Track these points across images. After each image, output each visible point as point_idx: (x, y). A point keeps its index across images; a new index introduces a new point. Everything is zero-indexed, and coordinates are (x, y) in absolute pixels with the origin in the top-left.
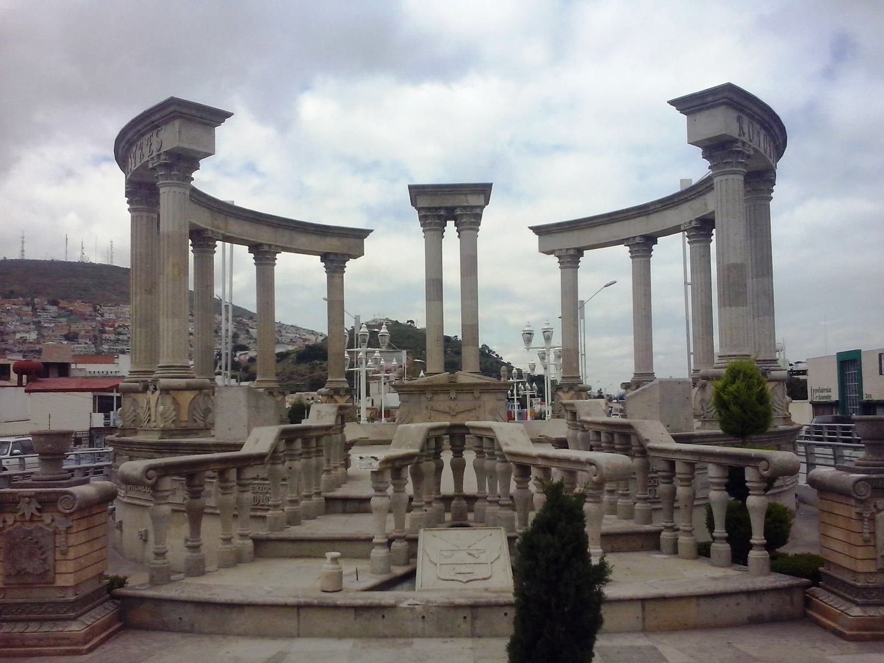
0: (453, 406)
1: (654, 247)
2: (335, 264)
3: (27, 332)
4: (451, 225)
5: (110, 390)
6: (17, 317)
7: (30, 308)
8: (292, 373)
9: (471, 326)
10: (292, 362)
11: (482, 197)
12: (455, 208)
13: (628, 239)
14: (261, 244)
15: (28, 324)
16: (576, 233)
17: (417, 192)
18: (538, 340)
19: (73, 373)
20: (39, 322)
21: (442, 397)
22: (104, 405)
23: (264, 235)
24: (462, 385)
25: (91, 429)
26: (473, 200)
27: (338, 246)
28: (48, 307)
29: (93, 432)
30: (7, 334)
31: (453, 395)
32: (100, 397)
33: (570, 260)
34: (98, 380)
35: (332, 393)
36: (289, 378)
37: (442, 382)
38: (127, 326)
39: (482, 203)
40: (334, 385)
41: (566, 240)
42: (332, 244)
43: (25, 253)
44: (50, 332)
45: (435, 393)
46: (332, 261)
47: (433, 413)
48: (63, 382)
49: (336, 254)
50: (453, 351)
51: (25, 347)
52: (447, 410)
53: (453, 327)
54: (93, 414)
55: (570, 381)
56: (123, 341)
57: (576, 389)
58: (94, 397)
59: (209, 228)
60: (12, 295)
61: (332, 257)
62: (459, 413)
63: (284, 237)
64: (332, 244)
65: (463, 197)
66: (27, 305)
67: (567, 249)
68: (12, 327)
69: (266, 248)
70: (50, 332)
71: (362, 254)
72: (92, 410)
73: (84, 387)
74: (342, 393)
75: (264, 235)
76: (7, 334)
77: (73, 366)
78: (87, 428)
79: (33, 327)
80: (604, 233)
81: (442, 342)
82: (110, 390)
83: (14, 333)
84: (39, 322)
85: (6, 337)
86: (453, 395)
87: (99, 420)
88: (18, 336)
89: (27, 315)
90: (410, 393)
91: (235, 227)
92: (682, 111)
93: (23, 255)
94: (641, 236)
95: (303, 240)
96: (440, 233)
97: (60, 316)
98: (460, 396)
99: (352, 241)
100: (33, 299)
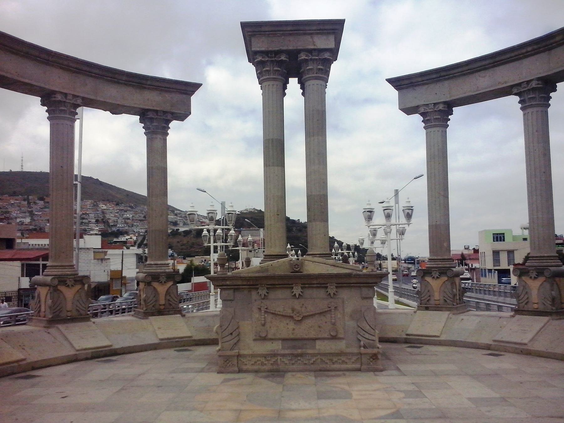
0: (297, 307)
1: (552, 94)
2: (156, 123)
3: (24, 218)
5: (37, 259)
6: (18, 208)
7: (26, 203)
8: (193, 244)
9: (318, 201)
10: (194, 237)
11: (332, 38)
12: (299, 51)
13: (519, 85)
14: (54, 92)
15: (25, 213)
16: (446, 83)
17: (253, 31)
18: (379, 219)
20: (32, 211)
21: (280, 294)
22: (30, 270)
23: (58, 81)
24: (310, 277)
25: (20, 289)
26: (322, 42)
27: (161, 103)
28: (38, 202)
29: (21, 292)
30: (12, 219)
31: (297, 290)
32: (27, 264)
33: (436, 117)
34: (28, 252)
35: (149, 279)
36: (191, 247)
37: (279, 273)
38: (88, 214)
39: (332, 45)
40: (153, 270)
41: (434, 95)
42: (152, 99)
43: (23, 167)
44: (39, 218)
45: (272, 287)
46: (151, 120)
47: (269, 318)
49: (156, 111)
50: (296, 234)
51: (23, 227)
52: (289, 312)
53: (297, 209)
54: (21, 278)
55: (441, 264)
56: (85, 223)
57: (449, 273)
58: (23, 265)
60: (14, 194)
61: (151, 115)
62: (305, 317)
63: (85, 86)
64: (152, 99)
65: (308, 38)
66: (24, 200)
67: (435, 104)
68: (15, 215)
69: (59, 97)
70: (39, 218)
72: (20, 275)
73: (16, 257)
74: (163, 279)
76: (12, 219)
77: (18, 241)
78: (16, 288)
79: (27, 214)
80: (484, 81)
81: (284, 221)
82: (37, 259)
83: (16, 218)
84: (32, 211)
85: (10, 221)
86: (297, 290)
87: (25, 283)
88: (18, 220)
89: (24, 207)
90: (236, 289)
93: (22, 168)
94: (539, 79)
95: (112, 92)
96: (280, 84)
97: (45, 207)
98: (308, 292)
99: (176, 97)
100: (28, 196)
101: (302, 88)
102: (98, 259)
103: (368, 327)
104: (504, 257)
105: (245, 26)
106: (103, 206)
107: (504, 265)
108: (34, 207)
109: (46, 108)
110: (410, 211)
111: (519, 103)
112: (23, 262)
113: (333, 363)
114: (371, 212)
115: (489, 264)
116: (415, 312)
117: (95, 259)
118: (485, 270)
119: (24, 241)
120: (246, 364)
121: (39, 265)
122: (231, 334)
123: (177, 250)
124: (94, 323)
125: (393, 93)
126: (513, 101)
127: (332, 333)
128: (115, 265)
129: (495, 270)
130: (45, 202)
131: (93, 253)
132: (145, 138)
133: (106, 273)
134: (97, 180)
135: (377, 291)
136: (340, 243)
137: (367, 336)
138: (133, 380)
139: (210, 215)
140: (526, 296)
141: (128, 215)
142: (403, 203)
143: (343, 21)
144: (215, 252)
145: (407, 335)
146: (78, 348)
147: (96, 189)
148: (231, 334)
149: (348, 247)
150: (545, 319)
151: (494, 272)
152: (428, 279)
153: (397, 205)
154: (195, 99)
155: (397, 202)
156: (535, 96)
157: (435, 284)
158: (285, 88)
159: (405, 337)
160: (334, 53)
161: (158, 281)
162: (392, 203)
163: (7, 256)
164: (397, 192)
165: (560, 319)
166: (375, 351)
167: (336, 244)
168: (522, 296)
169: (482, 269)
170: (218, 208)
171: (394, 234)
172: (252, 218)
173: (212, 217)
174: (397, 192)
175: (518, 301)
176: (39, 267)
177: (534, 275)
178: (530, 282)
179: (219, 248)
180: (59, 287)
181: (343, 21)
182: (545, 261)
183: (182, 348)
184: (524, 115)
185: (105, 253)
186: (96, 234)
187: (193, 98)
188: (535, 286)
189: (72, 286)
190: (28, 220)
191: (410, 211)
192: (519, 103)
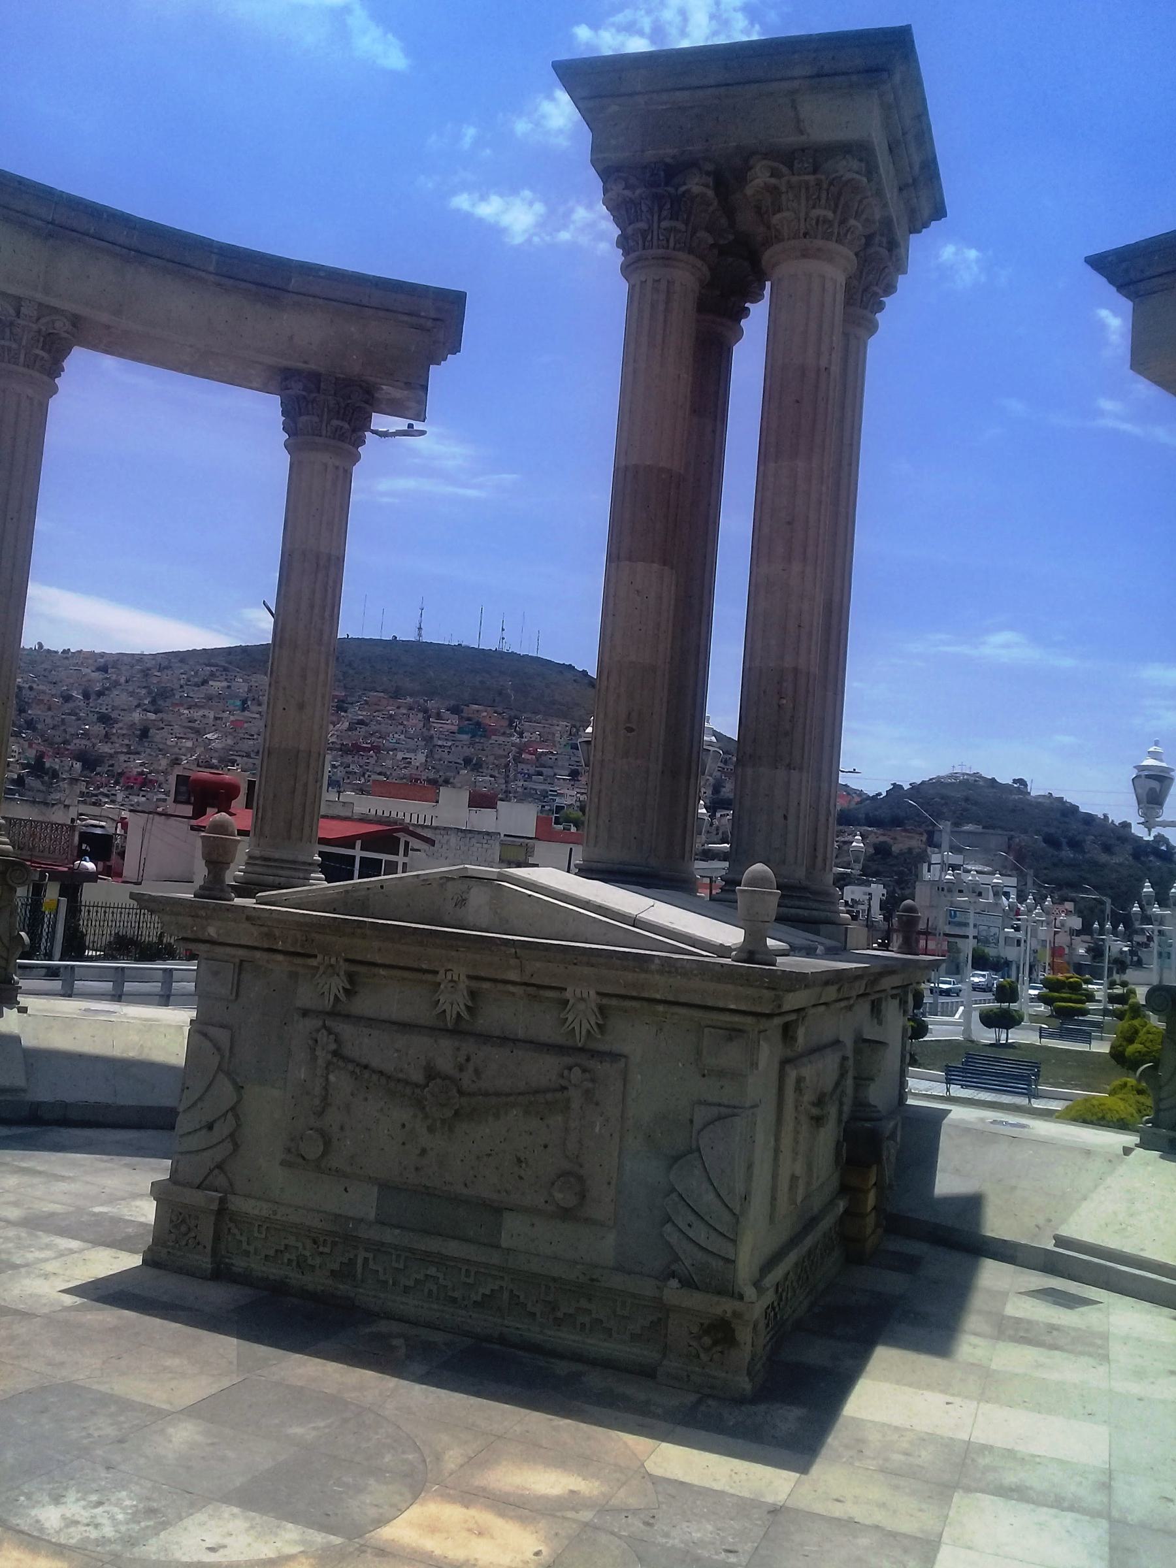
3: (414, 751)
5: (348, 842)
20: (432, 737)
63: (80, 280)
93: (420, 635)
97: (461, 731)
103: (711, 1196)
113: (558, 1322)
116: (1127, 1151)
120: (247, 1254)
121: (354, 857)
122: (210, 1127)
124: (23, 1010)
125: (1114, 319)
130: (461, 718)
132: (286, 458)
137: (701, 1234)
145: (1060, 1241)
148: (210, 1127)
159: (1050, 1245)
166: (724, 1307)
176: (353, 865)
190: (420, 758)
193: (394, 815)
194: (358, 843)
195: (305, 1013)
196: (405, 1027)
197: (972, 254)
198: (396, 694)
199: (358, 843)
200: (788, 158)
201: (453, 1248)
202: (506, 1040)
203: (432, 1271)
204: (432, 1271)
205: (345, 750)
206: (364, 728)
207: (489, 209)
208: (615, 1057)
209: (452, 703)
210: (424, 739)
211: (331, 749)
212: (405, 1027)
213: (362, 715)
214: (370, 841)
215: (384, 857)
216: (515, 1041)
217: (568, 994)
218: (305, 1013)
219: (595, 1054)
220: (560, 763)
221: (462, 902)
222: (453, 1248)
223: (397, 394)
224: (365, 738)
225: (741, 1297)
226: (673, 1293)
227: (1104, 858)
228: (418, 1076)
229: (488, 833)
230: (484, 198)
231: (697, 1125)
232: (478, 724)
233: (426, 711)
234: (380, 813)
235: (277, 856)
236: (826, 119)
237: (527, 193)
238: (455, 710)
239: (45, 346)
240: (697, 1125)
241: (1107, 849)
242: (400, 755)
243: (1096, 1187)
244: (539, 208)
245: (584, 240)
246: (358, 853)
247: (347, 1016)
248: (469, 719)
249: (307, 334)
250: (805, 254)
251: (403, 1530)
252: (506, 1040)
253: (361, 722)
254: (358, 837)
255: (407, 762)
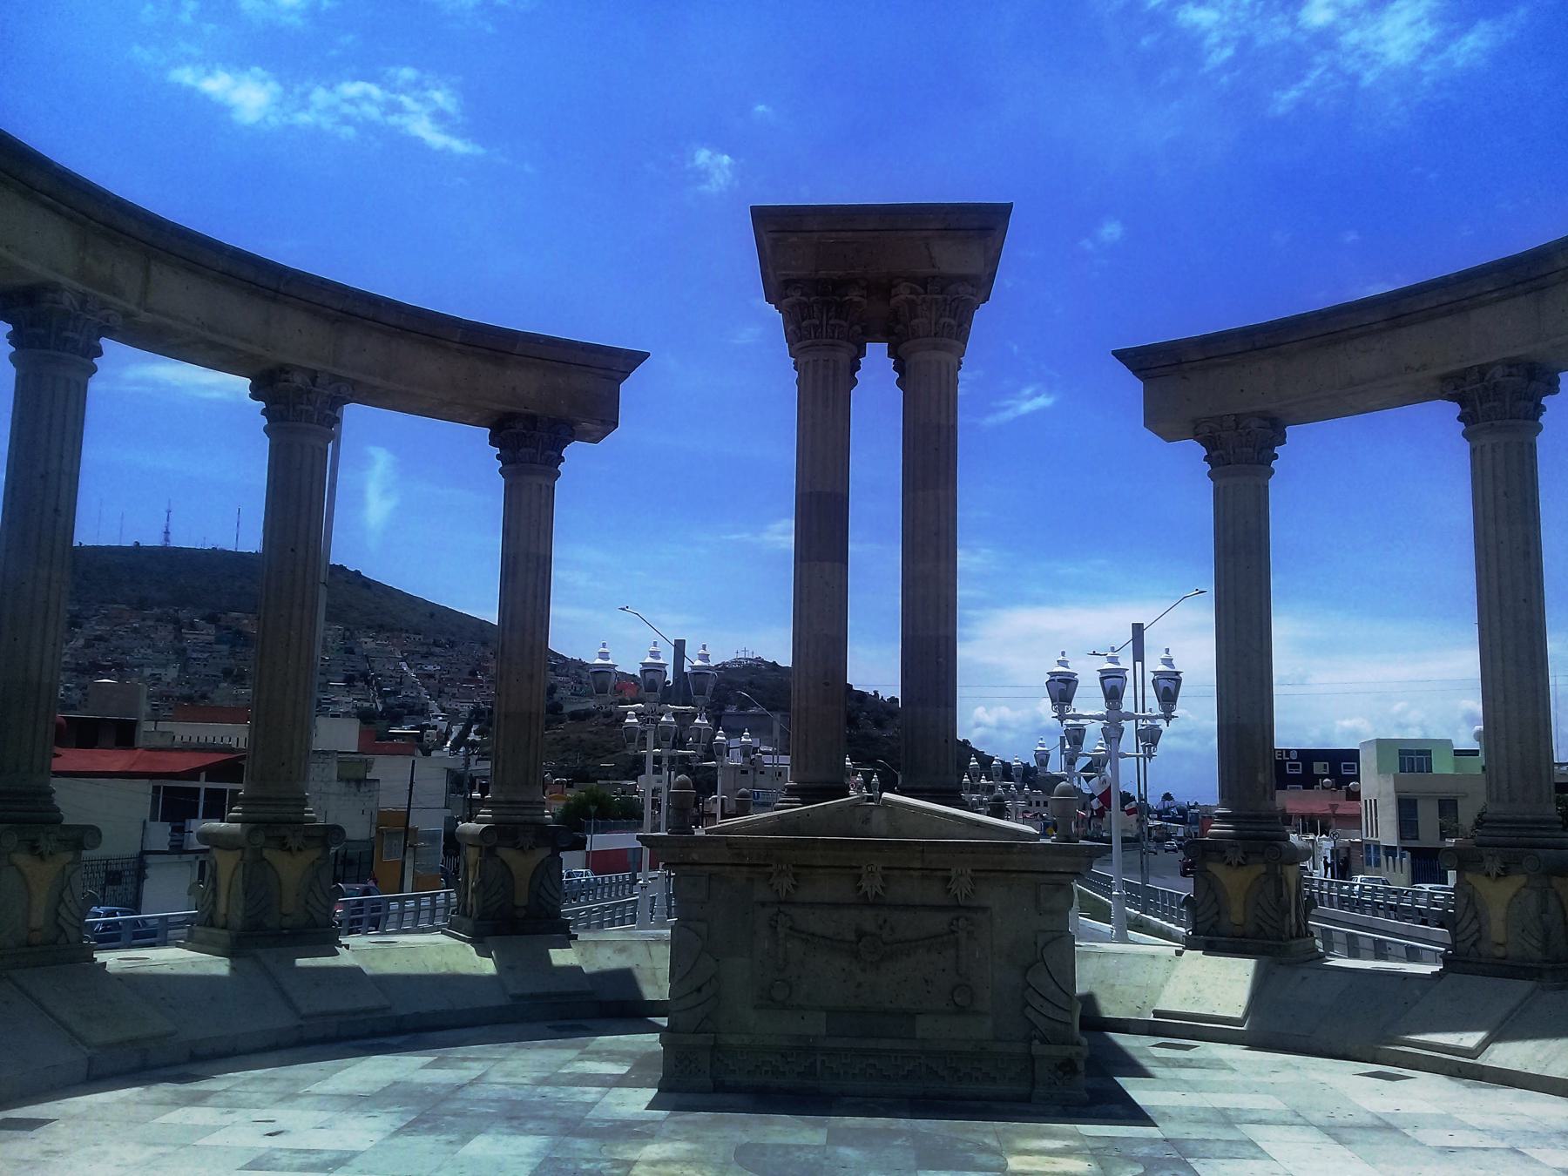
3: (165, 666)
4: (877, 359)
5: (193, 774)
19: (140, 740)
20: (184, 650)
27: (542, 405)
33: (1241, 454)
48: (117, 760)
58: (156, 789)
59: (64, 280)
69: (298, 379)
71: (610, 422)
75: (298, 340)
77: (147, 726)
91: (177, 294)
92: (1137, 371)
93: (167, 540)
97: (218, 641)
101: (900, 367)
102: (348, 781)
103: (1053, 987)
104: (1428, 819)
105: (764, 218)
106: (368, 643)
107: (1428, 836)
108: (190, 637)
109: (262, 405)
110: (1171, 685)
111: (1460, 419)
112: (157, 782)
114: (1067, 682)
115: (1388, 835)
116: (1179, 953)
117: (340, 779)
118: (1377, 847)
119: (164, 726)
122: (699, 990)
123: (546, 760)
124: (347, 947)
125: (1132, 388)
126: (1442, 417)
127: (957, 1000)
128: (391, 799)
129: (1404, 849)
130: (218, 628)
131: (335, 764)
133: (367, 817)
134: (358, 573)
135: (1080, 891)
136: (986, 761)
138: (445, 1099)
139: (649, 676)
140: (1474, 926)
141: (430, 667)
142: (1153, 663)
143: (1003, 211)
144: (657, 771)
145: (1157, 1013)
146: (304, 1011)
147: (374, 608)
148: (699, 990)
149: (1007, 770)
150: (1524, 986)
151: (1402, 856)
152: (1217, 869)
153: (1139, 664)
154: (628, 390)
155: (1139, 655)
156: (1497, 408)
157: (1235, 881)
158: (855, 367)
160: (982, 285)
161: (514, 846)
162: (1126, 661)
163: (116, 767)
164: (1138, 630)
165: (1561, 988)
166: (1070, 1051)
167: (974, 763)
168: (1464, 924)
169: (1368, 847)
170: (667, 658)
171: (1128, 742)
172: (751, 683)
173: (653, 681)
174: (1138, 630)
175: (1454, 935)
176: (197, 797)
177: (1494, 866)
178: (1483, 885)
179: (665, 762)
180: (266, 853)
181: (1003, 211)
182: (1537, 833)
183: (568, 1023)
184: (1473, 451)
185: (368, 766)
186: (347, 714)
187: (627, 389)
188: (1500, 896)
189: (299, 849)
190: (172, 673)
191: (1171, 685)
192: (1460, 419)
193: (210, 740)
194: (203, 775)
195: (763, 904)
196: (836, 905)
197: (726, 159)
198: (141, 604)
199: (203, 775)
200: (924, 282)
201: (886, 1044)
202: (907, 907)
203: (871, 1061)
204: (871, 1061)
205: (80, 670)
206: (103, 645)
207: (217, 84)
208: (984, 909)
209: (208, 611)
210: (176, 653)
211: (64, 670)
212: (836, 905)
213: (101, 629)
214: (214, 772)
215: (228, 786)
216: (914, 906)
217: (953, 873)
218: (763, 904)
219: (968, 908)
220: (333, 669)
221: (867, 821)
222: (886, 1044)
223: (587, 426)
224: (104, 655)
225: (1078, 1044)
226: (1037, 1047)
227: (875, 732)
228: (852, 937)
229: (324, 752)
230: (209, 73)
231: (1040, 944)
232: (239, 633)
233: (177, 622)
234: (202, 740)
235: (519, 799)
236: (950, 258)
237: (257, 70)
238: (212, 619)
239: (338, 402)
240: (1040, 944)
241: (879, 724)
242: (147, 672)
243: (1167, 979)
244: (274, 87)
245: (327, 123)
246: (203, 784)
247: (793, 903)
248: (228, 628)
249: (522, 386)
250: (936, 348)
251: (1015, 1163)
252: (907, 907)
253: (100, 638)
254: (205, 768)
255: (157, 679)
